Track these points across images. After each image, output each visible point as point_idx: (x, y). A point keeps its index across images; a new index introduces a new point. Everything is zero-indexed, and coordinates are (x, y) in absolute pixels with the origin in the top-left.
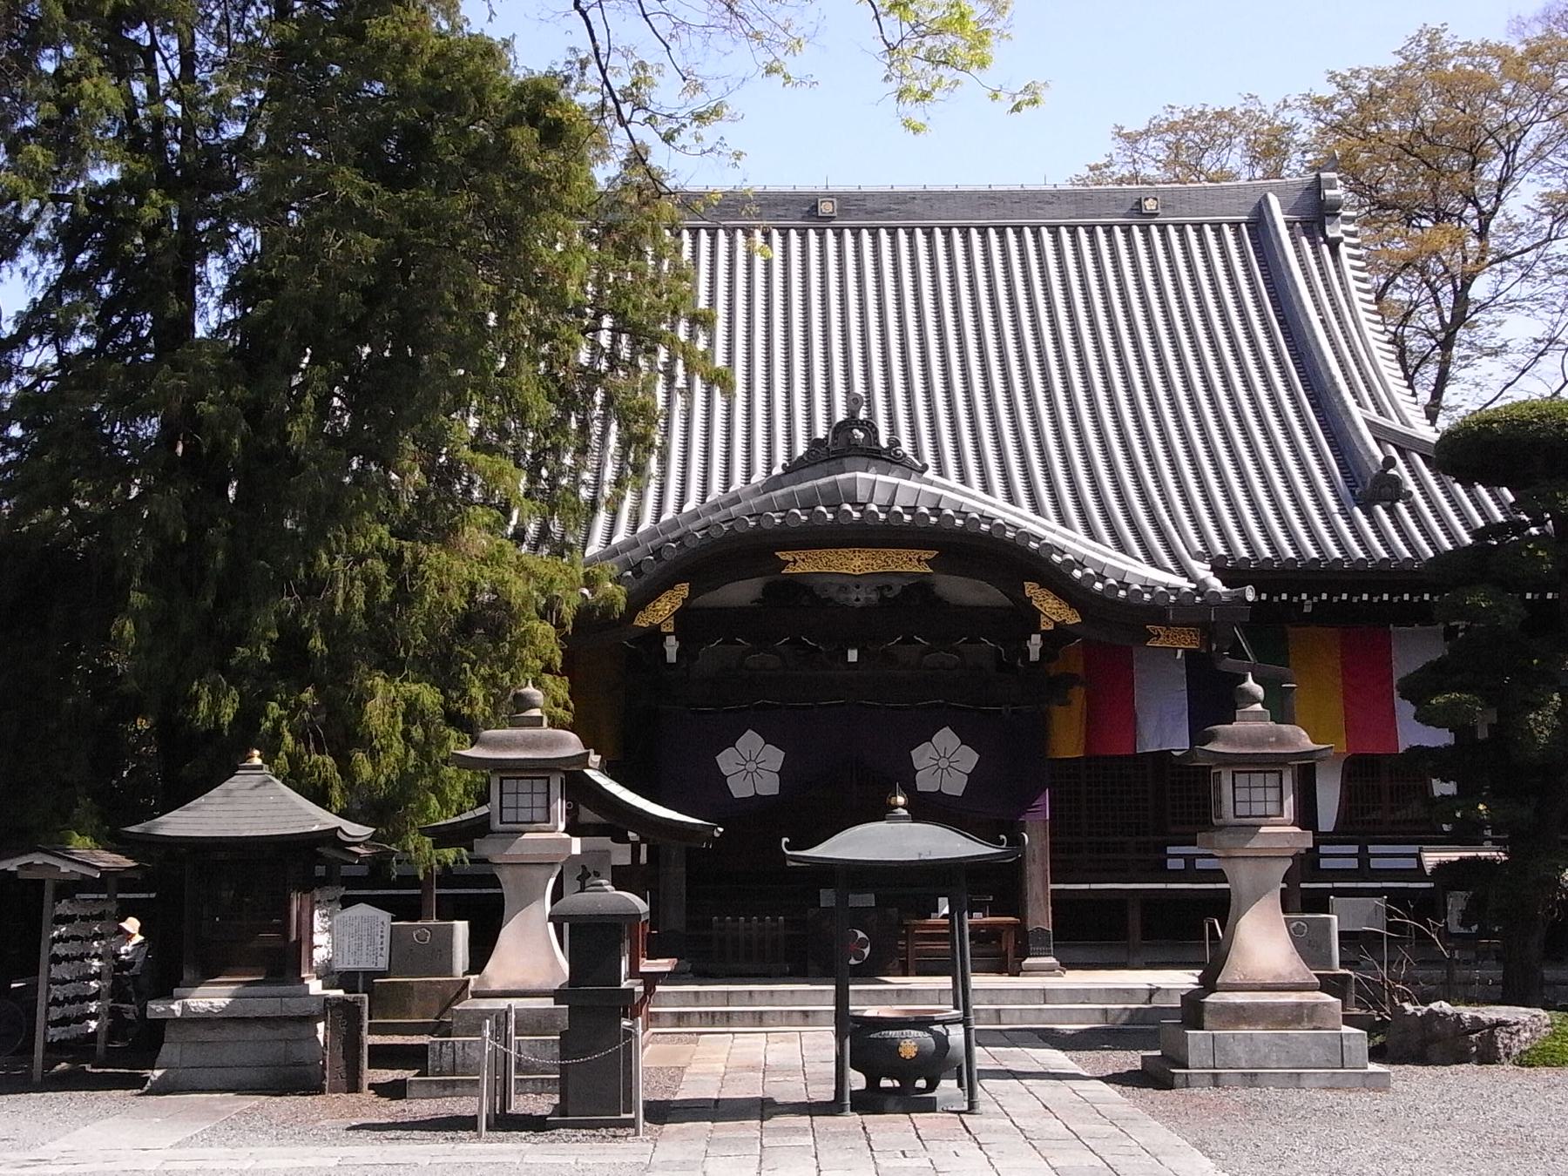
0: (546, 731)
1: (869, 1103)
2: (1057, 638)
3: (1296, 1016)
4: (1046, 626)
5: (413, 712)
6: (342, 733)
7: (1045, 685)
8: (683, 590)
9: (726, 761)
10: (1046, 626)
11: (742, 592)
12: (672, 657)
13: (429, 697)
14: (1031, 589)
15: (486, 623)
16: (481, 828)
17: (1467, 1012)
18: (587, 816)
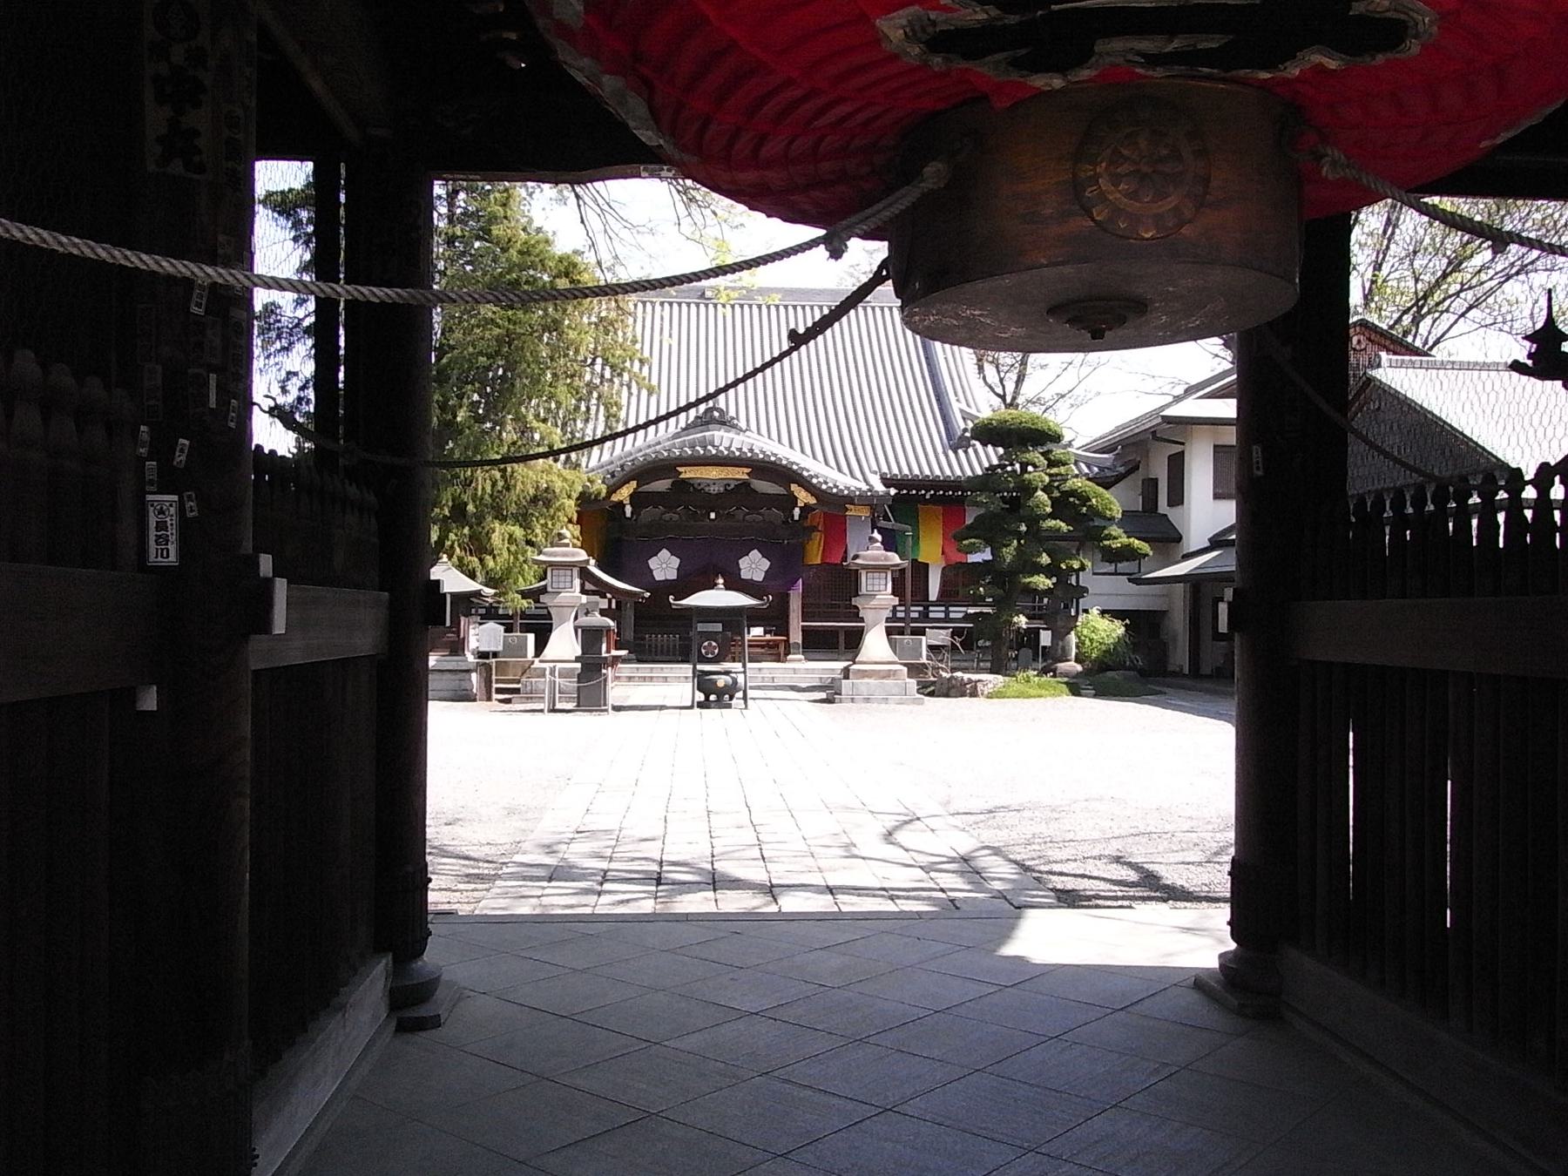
0: (571, 549)
1: (701, 705)
2: (806, 509)
3: (888, 675)
4: (800, 504)
5: (512, 539)
6: (479, 546)
7: (802, 530)
8: (634, 484)
9: (653, 563)
10: (800, 504)
11: (662, 485)
12: (628, 514)
13: (518, 532)
14: (794, 487)
15: (544, 499)
16: (544, 590)
17: (966, 676)
18: (589, 586)
